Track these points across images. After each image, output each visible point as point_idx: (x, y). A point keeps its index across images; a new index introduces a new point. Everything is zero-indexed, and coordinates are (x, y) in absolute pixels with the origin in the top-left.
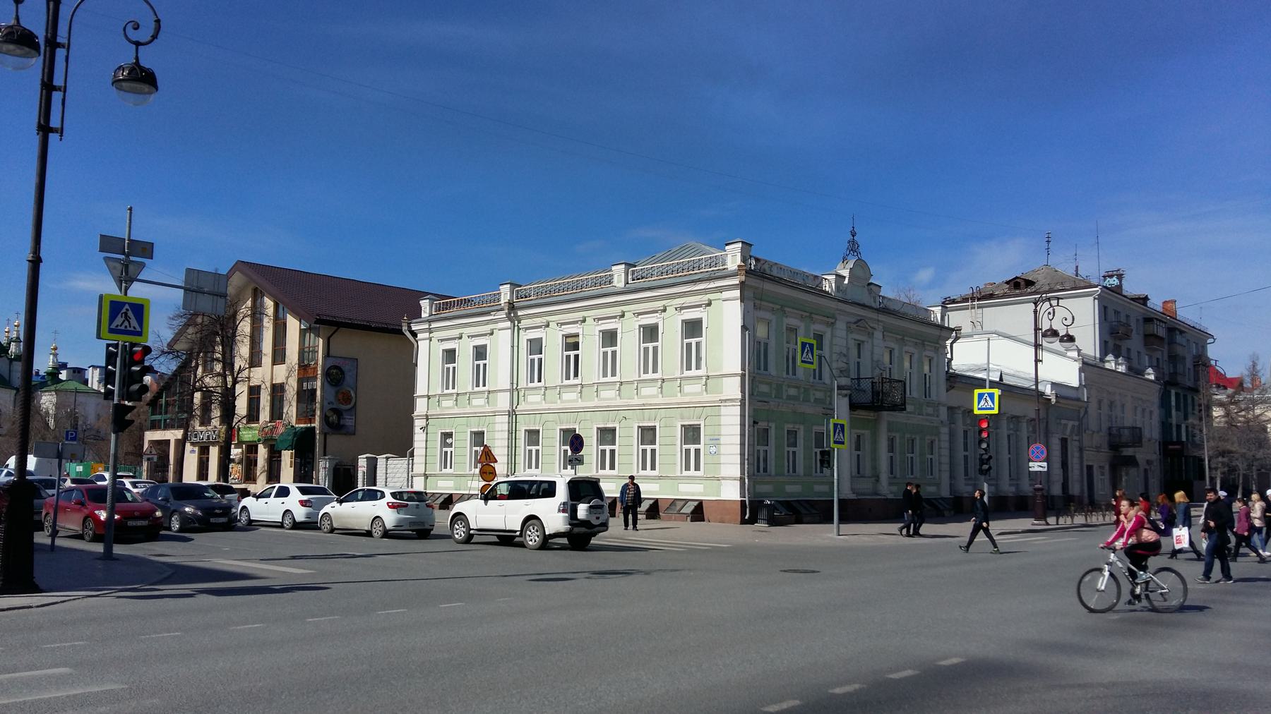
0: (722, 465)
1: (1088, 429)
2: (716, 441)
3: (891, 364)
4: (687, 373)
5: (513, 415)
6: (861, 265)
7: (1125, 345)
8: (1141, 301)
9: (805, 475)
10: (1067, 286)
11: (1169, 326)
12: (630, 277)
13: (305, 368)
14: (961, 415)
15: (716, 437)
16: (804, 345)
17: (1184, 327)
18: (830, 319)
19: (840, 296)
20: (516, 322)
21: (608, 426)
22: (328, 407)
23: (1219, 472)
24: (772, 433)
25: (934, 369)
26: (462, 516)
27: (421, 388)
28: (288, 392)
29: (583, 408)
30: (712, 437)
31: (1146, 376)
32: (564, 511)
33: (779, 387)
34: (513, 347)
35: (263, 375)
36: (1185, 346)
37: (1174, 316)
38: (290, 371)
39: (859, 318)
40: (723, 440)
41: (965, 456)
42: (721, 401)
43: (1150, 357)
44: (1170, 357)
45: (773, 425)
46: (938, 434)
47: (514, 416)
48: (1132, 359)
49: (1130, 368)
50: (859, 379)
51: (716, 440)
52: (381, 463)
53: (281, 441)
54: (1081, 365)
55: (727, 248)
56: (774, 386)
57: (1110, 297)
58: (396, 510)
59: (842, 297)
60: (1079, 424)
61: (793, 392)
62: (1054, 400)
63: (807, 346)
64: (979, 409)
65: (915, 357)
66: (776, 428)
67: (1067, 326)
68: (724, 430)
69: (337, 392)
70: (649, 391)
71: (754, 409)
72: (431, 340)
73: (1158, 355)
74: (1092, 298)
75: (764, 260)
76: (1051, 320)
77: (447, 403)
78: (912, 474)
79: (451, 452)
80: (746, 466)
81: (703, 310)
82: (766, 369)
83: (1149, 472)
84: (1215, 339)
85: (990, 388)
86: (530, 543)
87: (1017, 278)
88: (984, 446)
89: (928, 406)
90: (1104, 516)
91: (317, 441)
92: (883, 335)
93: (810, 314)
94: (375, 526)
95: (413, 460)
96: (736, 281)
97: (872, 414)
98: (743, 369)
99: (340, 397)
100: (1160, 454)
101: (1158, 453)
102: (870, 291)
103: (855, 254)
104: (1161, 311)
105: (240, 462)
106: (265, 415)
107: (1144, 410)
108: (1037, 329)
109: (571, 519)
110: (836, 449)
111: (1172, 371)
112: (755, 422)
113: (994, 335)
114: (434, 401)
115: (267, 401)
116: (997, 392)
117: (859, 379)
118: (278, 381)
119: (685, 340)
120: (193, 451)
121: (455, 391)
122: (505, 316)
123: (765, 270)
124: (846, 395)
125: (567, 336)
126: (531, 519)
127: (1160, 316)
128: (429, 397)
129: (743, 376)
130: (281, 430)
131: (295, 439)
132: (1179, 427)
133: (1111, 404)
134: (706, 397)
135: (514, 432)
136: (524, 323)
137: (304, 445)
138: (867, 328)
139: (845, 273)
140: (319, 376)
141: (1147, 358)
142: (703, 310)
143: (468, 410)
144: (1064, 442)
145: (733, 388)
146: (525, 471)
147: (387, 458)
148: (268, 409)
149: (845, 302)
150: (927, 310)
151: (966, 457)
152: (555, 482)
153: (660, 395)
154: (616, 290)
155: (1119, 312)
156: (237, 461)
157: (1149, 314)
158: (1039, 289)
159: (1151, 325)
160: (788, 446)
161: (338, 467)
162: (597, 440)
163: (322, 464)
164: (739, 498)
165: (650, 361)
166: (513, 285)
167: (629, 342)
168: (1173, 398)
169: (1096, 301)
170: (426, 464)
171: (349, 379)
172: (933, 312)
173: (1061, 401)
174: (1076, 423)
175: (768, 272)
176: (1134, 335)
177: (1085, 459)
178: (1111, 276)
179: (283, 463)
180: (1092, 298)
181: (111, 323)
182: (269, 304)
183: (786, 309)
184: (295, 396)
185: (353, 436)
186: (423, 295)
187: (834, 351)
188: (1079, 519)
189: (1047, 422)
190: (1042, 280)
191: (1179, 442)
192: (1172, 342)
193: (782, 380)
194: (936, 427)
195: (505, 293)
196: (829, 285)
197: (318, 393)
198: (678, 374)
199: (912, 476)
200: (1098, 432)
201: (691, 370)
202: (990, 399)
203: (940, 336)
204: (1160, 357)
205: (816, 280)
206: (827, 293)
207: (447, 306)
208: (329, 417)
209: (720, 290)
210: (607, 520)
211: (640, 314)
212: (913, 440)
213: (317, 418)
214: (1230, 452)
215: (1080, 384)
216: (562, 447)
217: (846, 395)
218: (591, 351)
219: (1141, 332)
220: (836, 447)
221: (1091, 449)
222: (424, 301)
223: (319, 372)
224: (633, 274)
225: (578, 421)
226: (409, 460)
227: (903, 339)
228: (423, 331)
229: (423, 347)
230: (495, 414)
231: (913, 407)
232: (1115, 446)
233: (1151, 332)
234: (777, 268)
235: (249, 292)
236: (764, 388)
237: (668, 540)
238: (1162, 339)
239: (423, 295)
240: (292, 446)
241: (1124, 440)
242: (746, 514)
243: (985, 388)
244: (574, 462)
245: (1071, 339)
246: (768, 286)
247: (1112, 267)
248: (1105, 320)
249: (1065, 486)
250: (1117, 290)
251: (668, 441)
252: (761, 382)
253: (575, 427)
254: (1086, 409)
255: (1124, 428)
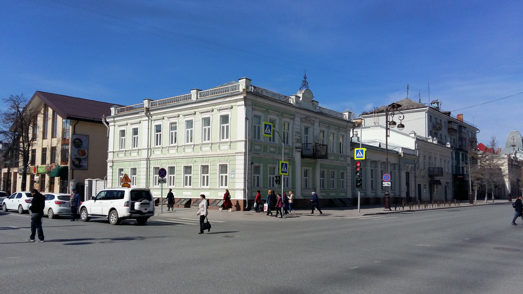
0: (236, 183)
1: (419, 168)
2: (234, 172)
3: (323, 138)
4: (222, 140)
5: (148, 160)
6: (308, 91)
7: (439, 132)
8: (448, 114)
9: (278, 188)
10: (415, 107)
11: (459, 125)
12: (199, 95)
13: (64, 141)
14: (380, 164)
15: (234, 170)
16: (266, 125)
17: (466, 125)
18: (293, 117)
19: (297, 106)
20: (150, 117)
21: (188, 165)
22: (74, 157)
23: (476, 187)
24: (261, 169)
25: (345, 140)
26: (84, 208)
27: (110, 149)
28: (57, 150)
29: (178, 157)
30: (232, 170)
31: (447, 146)
32: (127, 206)
33: (265, 148)
34: (148, 129)
35: (47, 143)
36: (466, 134)
37: (462, 121)
38: (58, 141)
39: (307, 116)
40: (237, 171)
41: (371, 180)
42: (236, 153)
43: (451, 138)
44: (459, 138)
45: (262, 165)
46: (346, 170)
47: (149, 161)
48: (442, 139)
49: (439, 142)
50: (307, 144)
51: (234, 171)
52: (94, 183)
53: (53, 173)
54: (416, 140)
55: (239, 81)
56: (263, 146)
57: (434, 112)
58: (59, 205)
59: (298, 106)
60: (415, 166)
61: (272, 149)
62: (402, 155)
63: (268, 126)
64: (357, 157)
65: (335, 135)
66: (263, 166)
67: (401, 120)
68: (237, 167)
69: (78, 151)
70: (206, 149)
71: (251, 157)
72: (115, 126)
73: (454, 137)
74: (425, 112)
75: (258, 87)
76: (393, 117)
77: (121, 155)
78: (333, 187)
79: (136, 177)
80: (247, 184)
81: (229, 111)
82: (259, 138)
83: (447, 187)
84: (480, 131)
85: (362, 148)
86: (113, 222)
87: (393, 103)
88: (358, 174)
89: (341, 157)
90: (419, 207)
91: (69, 173)
92: (319, 124)
93: (282, 114)
94: (49, 213)
95: (107, 181)
96: (242, 97)
97: (313, 160)
98: (246, 138)
99: (80, 152)
100: (452, 179)
101: (451, 179)
102: (313, 104)
103: (306, 87)
104: (456, 118)
105: (38, 182)
106: (48, 161)
107: (445, 160)
108: (387, 122)
109: (131, 210)
110: (283, 175)
111: (460, 144)
112: (252, 163)
113: (379, 127)
114: (116, 154)
115: (49, 155)
116: (364, 150)
117: (307, 144)
118: (54, 145)
119: (222, 125)
120: (20, 177)
121: (125, 149)
122: (144, 114)
123: (259, 92)
124: (299, 151)
125: (171, 124)
126: (113, 209)
127: (456, 121)
128: (114, 152)
129: (246, 141)
130: (54, 167)
131: (58, 172)
132: (463, 168)
133: (430, 158)
134: (230, 152)
135: (149, 168)
136: (154, 117)
137: (63, 173)
138: (310, 121)
139: (300, 95)
140: (70, 143)
141: (449, 138)
142: (229, 111)
143: (130, 158)
144: (408, 174)
145: (241, 147)
146: (153, 186)
147: (97, 181)
148: (49, 158)
149: (300, 108)
150: (342, 114)
151: (372, 181)
152: (124, 191)
153: (211, 151)
154: (192, 101)
155: (437, 119)
156: (37, 182)
157: (450, 119)
158: (403, 108)
159: (451, 124)
160: (331, 178)
161: (78, 184)
162: (184, 172)
163: (71, 183)
164: (243, 199)
165: (207, 134)
166: (149, 100)
167: (198, 126)
168: (461, 156)
169: (427, 113)
170: (112, 183)
171: (84, 144)
172: (345, 115)
173: (406, 156)
174: (413, 166)
175: (260, 93)
176: (443, 128)
177: (417, 181)
178: (434, 103)
179: (55, 183)
180: (425, 112)
181: (356, 156)
182: (50, 111)
183: (269, 111)
184: (60, 152)
185: (86, 171)
186: (112, 105)
187: (294, 131)
188: (407, 208)
189: (399, 165)
190: (404, 105)
191: (463, 175)
192: (460, 132)
193: (267, 144)
194: (345, 166)
195: (146, 103)
196: (292, 100)
197: (70, 151)
198: (218, 141)
199: (333, 189)
200: (423, 170)
201: (224, 139)
202: (362, 153)
203: (347, 126)
204: (455, 138)
205: (286, 98)
206: (292, 104)
207: (122, 111)
208: (74, 162)
209: (236, 101)
210: (154, 209)
211: (202, 113)
212: (334, 172)
213: (69, 162)
214: (481, 179)
215: (415, 148)
216: (169, 175)
217: (299, 151)
218: (181, 130)
219: (447, 128)
220: (283, 174)
221: (421, 177)
222: (112, 108)
223: (70, 141)
224: (200, 95)
225: (176, 163)
226: (105, 181)
227: (329, 126)
228: (111, 122)
229: (111, 129)
230: (141, 160)
231: (334, 157)
232: (431, 176)
233: (451, 127)
234: (265, 91)
235: (43, 106)
236: (258, 147)
237: (188, 218)
238: (456, 130)
239: (112, 105)
240: (57, 175)
241: (435, 173)
242: (246, 206)
243: (359, 147)
244: (161, 182)
245: (403, 126)
246: (259, 100)
247: (434, 99)
248: (431, 122)
249: (408, 193)
250: (437, 109)
251: (214, 172)
252: (256, 145)
253: (174, 166)
254: (418, 159)
255: (435, 168)
